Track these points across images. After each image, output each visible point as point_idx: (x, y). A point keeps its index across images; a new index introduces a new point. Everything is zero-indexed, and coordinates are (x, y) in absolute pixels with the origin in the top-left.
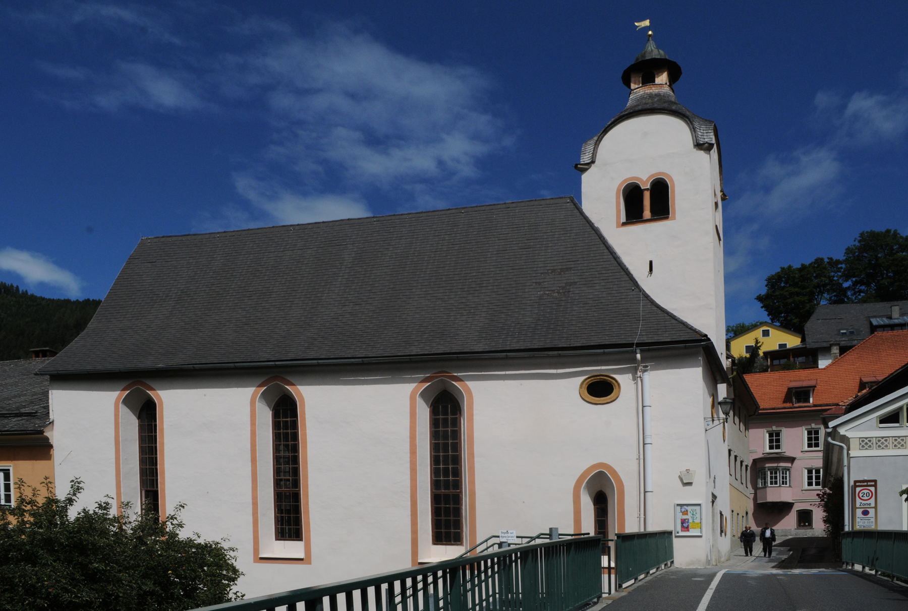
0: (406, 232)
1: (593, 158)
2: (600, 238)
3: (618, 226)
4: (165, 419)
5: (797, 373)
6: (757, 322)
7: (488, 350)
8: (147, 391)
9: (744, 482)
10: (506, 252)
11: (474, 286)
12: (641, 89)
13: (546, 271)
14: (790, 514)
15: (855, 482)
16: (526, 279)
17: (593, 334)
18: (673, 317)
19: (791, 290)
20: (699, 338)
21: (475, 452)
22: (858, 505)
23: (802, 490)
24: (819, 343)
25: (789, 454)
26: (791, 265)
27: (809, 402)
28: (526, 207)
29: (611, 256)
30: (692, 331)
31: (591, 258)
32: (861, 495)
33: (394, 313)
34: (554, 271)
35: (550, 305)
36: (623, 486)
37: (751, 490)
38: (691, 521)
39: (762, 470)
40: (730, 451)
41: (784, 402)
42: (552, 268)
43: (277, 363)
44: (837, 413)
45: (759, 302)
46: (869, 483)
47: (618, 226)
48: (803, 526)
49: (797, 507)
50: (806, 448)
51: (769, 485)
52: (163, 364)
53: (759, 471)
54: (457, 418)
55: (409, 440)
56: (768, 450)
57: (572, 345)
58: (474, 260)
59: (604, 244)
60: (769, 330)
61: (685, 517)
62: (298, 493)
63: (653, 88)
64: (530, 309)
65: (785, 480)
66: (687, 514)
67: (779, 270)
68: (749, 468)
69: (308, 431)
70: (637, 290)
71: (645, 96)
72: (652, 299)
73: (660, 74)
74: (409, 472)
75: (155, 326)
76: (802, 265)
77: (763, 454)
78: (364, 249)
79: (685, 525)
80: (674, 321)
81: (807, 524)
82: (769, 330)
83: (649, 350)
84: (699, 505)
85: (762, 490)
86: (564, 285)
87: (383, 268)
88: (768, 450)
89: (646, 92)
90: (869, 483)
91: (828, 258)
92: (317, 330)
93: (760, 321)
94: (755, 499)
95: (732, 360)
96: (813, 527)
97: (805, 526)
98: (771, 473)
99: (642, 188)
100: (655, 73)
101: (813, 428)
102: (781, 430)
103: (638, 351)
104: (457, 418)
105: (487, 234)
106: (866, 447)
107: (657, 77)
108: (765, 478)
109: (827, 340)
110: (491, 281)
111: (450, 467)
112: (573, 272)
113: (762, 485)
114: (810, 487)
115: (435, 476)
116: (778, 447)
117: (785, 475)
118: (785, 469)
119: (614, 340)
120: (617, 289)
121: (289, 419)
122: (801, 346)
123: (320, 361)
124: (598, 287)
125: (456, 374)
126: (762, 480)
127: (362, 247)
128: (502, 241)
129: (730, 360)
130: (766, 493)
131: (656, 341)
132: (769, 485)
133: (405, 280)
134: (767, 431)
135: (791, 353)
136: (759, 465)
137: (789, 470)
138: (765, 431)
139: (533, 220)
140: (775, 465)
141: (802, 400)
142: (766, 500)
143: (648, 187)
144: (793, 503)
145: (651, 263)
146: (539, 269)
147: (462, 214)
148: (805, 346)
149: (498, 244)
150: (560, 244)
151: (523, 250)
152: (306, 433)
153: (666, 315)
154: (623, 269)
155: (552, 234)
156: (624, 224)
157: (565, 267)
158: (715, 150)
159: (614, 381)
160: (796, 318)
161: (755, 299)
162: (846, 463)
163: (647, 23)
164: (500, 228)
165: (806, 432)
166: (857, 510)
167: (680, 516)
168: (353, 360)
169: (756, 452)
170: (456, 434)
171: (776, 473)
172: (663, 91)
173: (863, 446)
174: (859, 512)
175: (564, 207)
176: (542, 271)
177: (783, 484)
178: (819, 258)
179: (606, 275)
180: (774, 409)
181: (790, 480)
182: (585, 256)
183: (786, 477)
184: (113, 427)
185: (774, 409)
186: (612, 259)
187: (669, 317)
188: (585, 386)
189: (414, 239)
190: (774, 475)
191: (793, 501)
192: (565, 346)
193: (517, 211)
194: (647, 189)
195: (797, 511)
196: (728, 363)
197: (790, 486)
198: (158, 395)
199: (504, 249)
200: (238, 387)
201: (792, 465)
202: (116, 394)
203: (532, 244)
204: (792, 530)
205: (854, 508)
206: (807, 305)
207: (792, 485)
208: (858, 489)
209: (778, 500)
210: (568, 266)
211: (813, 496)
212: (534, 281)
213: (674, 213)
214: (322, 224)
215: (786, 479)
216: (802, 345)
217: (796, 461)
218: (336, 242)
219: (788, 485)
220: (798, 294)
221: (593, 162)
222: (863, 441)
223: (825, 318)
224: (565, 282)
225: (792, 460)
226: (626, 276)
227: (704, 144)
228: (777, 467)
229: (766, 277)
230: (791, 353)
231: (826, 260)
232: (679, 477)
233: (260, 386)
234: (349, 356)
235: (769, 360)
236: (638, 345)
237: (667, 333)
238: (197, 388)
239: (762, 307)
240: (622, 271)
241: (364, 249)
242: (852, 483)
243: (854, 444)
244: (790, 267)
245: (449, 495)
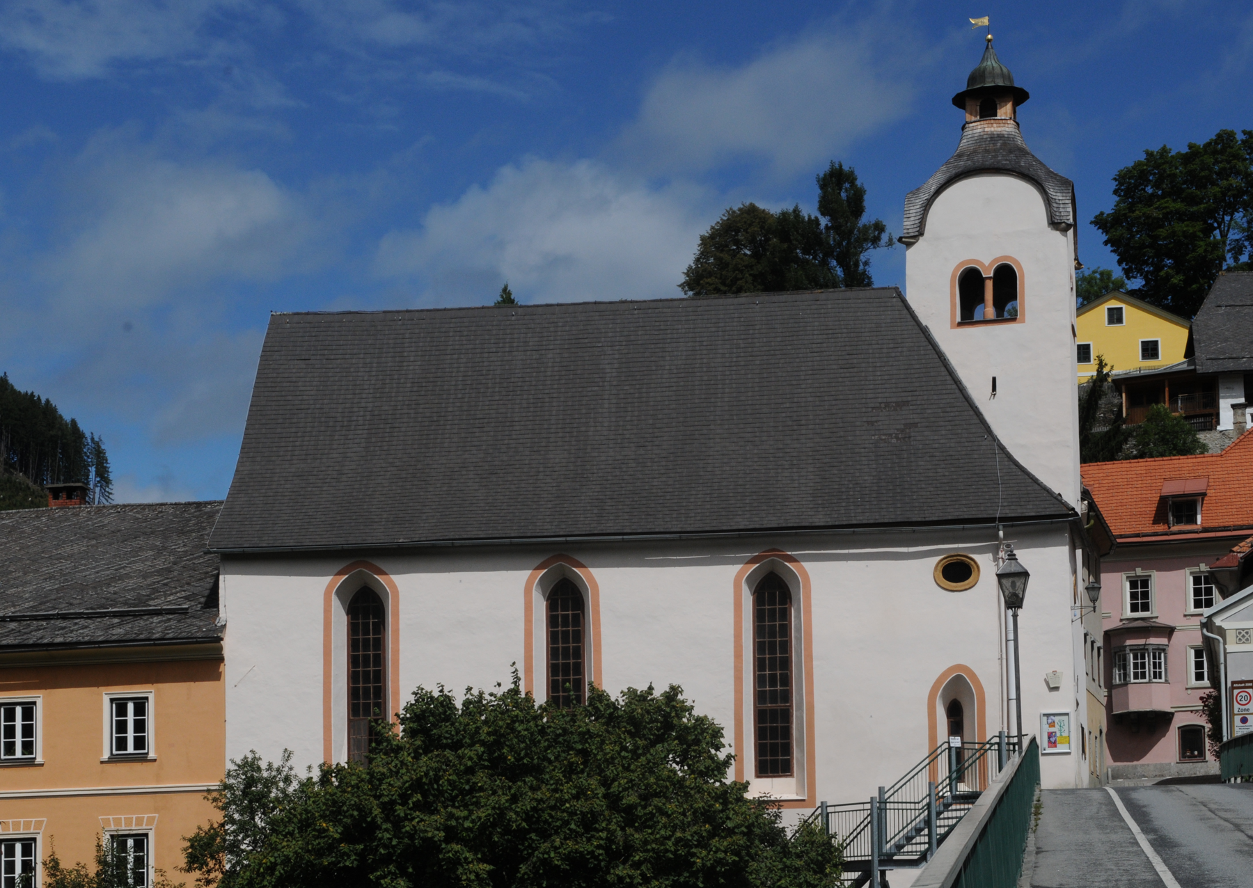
0: (684, 331)
1: (921, 229)
2: (940, 358)
3: (952, 327)
4: (401, 616)
5: (1175, 462)
6: (1094, 272)
7: (830, 524)
8: (376, 576)
9: (1096, 678)
10: (823, 372)
11: (790, 423)
12: (978, 123)
13: (878, 405)
14: (1167, 734)
15: (1233, 683)
16: (854, 415)
17: (948, 503)
18: (1035, 480)
19: (1166, 207)
20: (1064, 512)
21: (814, 654)
22: (1236, 712)
23: (1187, 689)
24: (1221, 361)
25: (1164, 620)
26: (1168, 147)
27: (1196, 524)
28: (840, 301)
29: (954, 386)
30: (1057, 502)
31: (930, 388)
32: (1239, 699)
33: (694, 462)
34: (887, 405)
35: (889, 457)
36: (984, 692)
37: (1104, 692)
38: (1058, 734)
39: (1121, 651)
40: (1086, 635)
41: (1156, 522)
42: (885, 400)
43: (568, 539)
44: (1229, 565)
45: (1101, 231)
46: (1247, 685)
47: (952, 327)
48: (1189, 757)
49: (1180, 721)
50: (1192, 610)
51: (1133, 681)
52: (404, 539)
53: (1115, 653)
54: (786, 608)
55: (733, 639)
56: (1129, 614)
57: (927, 519)
58: (784, 383)
59: (945, 367)
60: (1121, 308)
61: (1052, 730)
62: (788, 710)
63: (995, 125)
64: (866, 463)
65: (1158, 670)
66: (1054, 726)
67: (1142, 157)
68: (1102, 651)
69: (603, 630)
70: (990, 438)
71: (985, 137)
72: (1009, 453)
73: (1003, 104)
74: (732, 682)
75: (350, 471)
76: (1191, 146)
77: (1121, 620)
78: (630, 356)
79: (1053, 740)
80: (1036, 487)
81: (1196, 753)
82: (1121, 308)
83: (1012, 526)
84: (1067, 714)
85: (1120, 689)
86: (902, 427)
87: (664, 389)
88: (1129, 614)
89: (986, 130)
90: (1247, 685)
91: (1244, 132)
92: (599, 486)
93: (1101, 269)
94: (1109, 707)
95: (1089, 503)
96: (1207, 759)
97: (1193, 756)
98: (1135, 658)
99: (984, 276)
100: (998, 102)
101: (1203, 572)
102: (1150, 576)
103: (1001, 527)
104: (786, 608)
105: (796, 342)
106: (1244, 640)
107: (1000, 108)
108: (1124, 667)
109: (1234, 356)
110: (811, 417)
111: (778, 672)
112: (911, 407)
113: (1120, 680)
114: (1200, 683)
115: (353, 667)
116: (1146, 607)
117: (1158, 670)
118: (1158, 649)
119: (974, 513)
120: (966, 435)
121: (570, 612)
122: (1185, 367)
123: (625, 537)
124: (943, 432)
125: (789, 553)
126: (1119, 671)
127: (626, 351)
128: (815, 354)
129: (1086, 502)
130: (1127, 693)
131: (1020, 515)
132: (1132, 681)
133: (697, 410)
134: (1127, 577)
135: (1166, 384)
136: (1115, 642)
137: (1164, 650)
138: (1124, 577)
139: (851, 322)
140: (1141, 642)
141: (1184, 519)
142: (1128, 708)
143: (992, 275)
144: (1173, 714)
145: (994, 379)
146: (868, 400)
147: (755, 306)
148: (1192, 367)
149: (811, 359)
150: (890, 364)
151: (845, 370)
152: (600, 632)
153: (1027, 477)
154: (972, 408)
155: (879, 346)
156: (960, 324)
157: (900, 399)
158: (1071, 232)
159: (972, 563)
160: (1177, 273)
161: (1091, 223)
162: (1222, 660)
163: (985, 21)
164: (811, 333)
165: (1191, 579)
166: (1236, 717)
167: (1047, 729)
168: (668, 536)
169: (1109, 617)
170: (785, 630)
171: (1143, 657)
172: (1007, 129)
173: (1240, 639)
174: (1237, 719)
175: (890, 304)
176: (872, 405)
177: (1155, 677)
178: (1225, 132)
179: (952, 414)
180: (1138, 535)
181: (1166, 670)
182: (923, 384)
183: (1160, 663)
184: (321, 628)
185: (1138, 535)
186: (957, 391)
187: (1030, 480)
188: (940, 568)
189: (697, 344)
190: (1139, 670)
191: (1173, 710)
192: (919, 519)
193: (830, 306)
194: (990, 278)
195: (1179, 728)
196: (1083, 506)
197: (1167, 682)
198: (392, 581)
199: (821, 368)
200: (507, 569)
201: (1169, 641)
202: (327, 580)
203: (855, 361)
204: (1172, 764)
205: (1231, 715)
206: (1202, 243)
207: (1170, 679)
208: (1236, 692)
209: (1148, 709)
210: (905, 399)
211: (303, 776)
212: (865, 419)
213: (1023, 315)
214: (558, 308)
215: (1160, 668)
216: (1189, 363)
217: (1175, 634)
218: (586, 341)
219: (1163, 680)
220: (1181, 216)
221: (921, 234)
222: (1240, 633)
223: (1232, 303)
224: (903, 422)
225: (1169, 631)
226: (975, 417)
227: (1061, 223)
228: (1145, 645)
229: (1114, 172)
230: (1166, 384)
231: (1240, 137)
232: (1045, 680)
233: (539, 568)
234: (662, 530)
235: (1124, 395)
236: (1002, 520)
237: (1031, 503)
238: (449, 571)
239: (1106, 243)
240: (970, 409)
241: (630, 356)
242: (1229, 685)
243: (1230, 637)
244: (1164, 151)
245: (777, 710)
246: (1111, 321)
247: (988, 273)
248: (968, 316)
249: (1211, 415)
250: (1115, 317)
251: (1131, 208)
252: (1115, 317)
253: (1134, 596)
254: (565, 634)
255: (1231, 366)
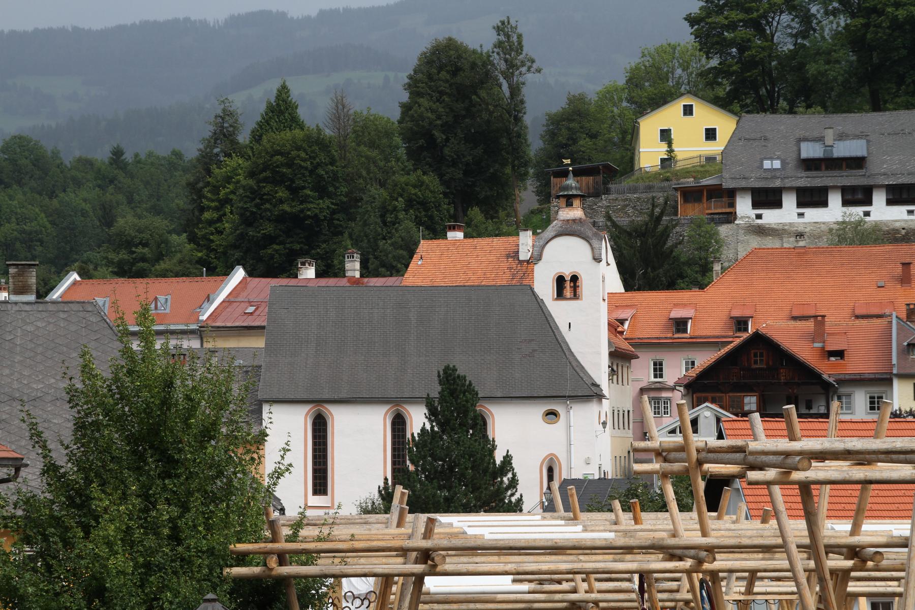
56: (652, 379)
60: (692, 106)
82: (692, 106)
88: (652, 379)
116: (661, 376)
156: (556, 299)
171: (659, 404)
246: (685, 114)
247: (568, 278)
248: (560, 295)
249: (731, 213)
250: (688, 111)
251: (709, 15)
252: (688, 111)
253: (655, 370)
254: (399, 435)
255: (743, 184)
